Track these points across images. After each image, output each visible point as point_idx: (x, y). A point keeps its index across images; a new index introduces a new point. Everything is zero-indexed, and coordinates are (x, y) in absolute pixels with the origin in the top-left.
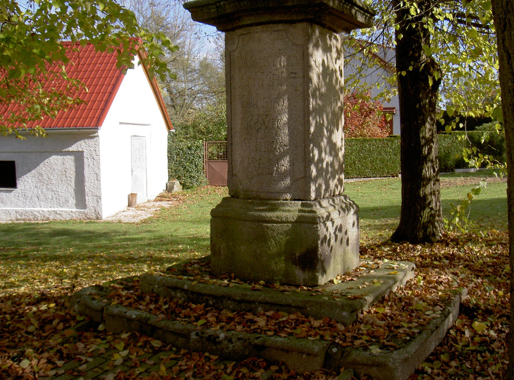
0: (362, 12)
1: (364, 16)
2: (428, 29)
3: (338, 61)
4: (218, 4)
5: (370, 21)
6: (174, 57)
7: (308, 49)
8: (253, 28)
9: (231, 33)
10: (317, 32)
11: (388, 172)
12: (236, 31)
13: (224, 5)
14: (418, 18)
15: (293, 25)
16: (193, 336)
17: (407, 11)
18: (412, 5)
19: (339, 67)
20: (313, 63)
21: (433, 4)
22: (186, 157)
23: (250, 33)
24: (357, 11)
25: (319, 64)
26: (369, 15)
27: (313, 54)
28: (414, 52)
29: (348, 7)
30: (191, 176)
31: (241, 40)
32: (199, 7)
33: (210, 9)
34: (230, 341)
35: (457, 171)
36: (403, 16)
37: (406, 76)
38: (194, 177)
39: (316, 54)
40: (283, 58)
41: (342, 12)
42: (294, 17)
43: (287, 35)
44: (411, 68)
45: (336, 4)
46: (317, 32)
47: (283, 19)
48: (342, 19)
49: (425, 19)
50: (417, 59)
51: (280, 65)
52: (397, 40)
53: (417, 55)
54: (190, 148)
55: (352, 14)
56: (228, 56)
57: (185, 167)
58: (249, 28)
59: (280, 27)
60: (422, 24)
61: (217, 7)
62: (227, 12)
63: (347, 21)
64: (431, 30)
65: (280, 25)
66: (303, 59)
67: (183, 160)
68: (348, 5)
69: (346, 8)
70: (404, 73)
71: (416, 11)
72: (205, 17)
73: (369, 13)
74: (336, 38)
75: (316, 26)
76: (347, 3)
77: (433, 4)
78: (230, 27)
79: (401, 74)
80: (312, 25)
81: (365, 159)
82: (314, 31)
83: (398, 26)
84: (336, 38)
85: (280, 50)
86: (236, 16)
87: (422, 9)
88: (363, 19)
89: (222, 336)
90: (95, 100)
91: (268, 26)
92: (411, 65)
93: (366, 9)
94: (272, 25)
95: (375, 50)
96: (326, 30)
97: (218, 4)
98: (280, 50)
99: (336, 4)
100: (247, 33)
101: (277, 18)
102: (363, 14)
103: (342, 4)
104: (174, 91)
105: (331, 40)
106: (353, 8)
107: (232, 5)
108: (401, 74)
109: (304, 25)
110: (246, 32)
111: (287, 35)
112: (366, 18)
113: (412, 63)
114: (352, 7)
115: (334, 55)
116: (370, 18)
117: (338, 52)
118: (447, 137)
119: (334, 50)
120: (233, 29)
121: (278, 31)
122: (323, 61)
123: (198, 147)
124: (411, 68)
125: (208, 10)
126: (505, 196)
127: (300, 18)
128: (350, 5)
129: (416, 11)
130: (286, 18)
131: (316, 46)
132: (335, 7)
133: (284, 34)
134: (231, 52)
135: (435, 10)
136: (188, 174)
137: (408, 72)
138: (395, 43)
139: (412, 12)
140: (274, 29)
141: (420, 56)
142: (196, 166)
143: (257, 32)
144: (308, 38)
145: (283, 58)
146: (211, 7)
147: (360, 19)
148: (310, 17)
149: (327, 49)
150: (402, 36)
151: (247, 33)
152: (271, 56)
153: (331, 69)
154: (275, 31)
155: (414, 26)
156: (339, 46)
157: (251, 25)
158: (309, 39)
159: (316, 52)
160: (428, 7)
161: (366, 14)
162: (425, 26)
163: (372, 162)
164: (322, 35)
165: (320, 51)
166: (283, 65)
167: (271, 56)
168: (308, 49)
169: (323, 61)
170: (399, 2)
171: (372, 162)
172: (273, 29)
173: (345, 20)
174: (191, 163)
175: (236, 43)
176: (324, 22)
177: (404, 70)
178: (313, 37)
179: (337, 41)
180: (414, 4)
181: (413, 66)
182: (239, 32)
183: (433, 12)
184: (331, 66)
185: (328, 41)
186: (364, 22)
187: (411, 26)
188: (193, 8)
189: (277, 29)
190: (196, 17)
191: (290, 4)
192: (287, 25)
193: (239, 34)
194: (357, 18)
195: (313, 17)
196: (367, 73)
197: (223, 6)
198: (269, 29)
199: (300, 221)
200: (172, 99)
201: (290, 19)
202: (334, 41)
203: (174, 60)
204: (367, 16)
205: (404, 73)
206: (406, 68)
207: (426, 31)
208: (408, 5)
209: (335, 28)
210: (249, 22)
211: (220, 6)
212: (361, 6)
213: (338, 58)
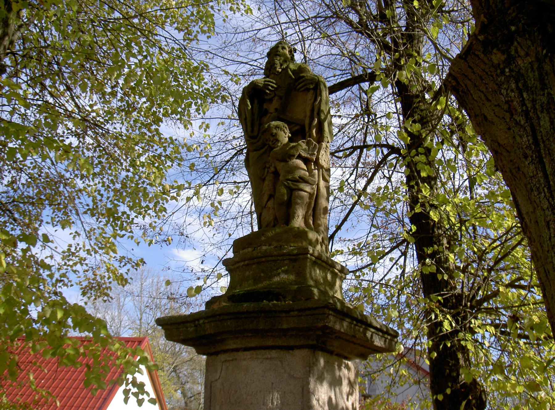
0: (381, 334)
1: (383, 339)
2: (466, 346)
3: (350, 397)
4: (197, 322)
5: (391, 344)
6: (191, 356)
7: (309, 384)
8: (240, 354)
9: (213, 357)
10: (322, 362)
12: (219, 356)
13: (204, 323)
14: (455, 333)
15: (291, 351)
17: (441, 324)
18: (445, 318)
19: (353, 404)
20: (315, 402)
21: (471, 316)
23: (236, 359)
24: (373, 333)
25: (324, 403)
26: (389, 337)
27: (314, 391)
28: (451, 371)
29: (361, 330)
31: (224, 367)
32: (174, 324)
33: (187, 328)
36: (437, 329)
37: (443, 400)
39: (320, 389)
40: (276, 395)
41: (354, 336)
42: (292, 342)
43: (282, 363)
44: (448, 391)
45: (345, 327)
46: (322, 362)
47: (277, 344)
48: (355, 344)
49: (461, 335)
50: (456, 379)
51: (272, 403)
52: (430, 359)
53: (455, 374)
55: (367, 338)
56: (209, 387)
58: (236, 353)
59: (274, 353)
60: (459, 341)
61: (196, 326)
62: (207, 333)
63: (362, 346)
64: (470, 346)
65: (274, 351)
66: (303, 396)
68: (361, 327)
69: (359, 331)
70: (440, 397)
71: (451, 325)
72: (182, 337)
73: (389, 334)
74: (349, 369)
75: (320, 353)
76: (359, 324)
77: (471, 316)
78: (213, 350)
79: (437, 398)
80: (314, 352)
82: (317, 360)
83: (431, 343)
84: (349, 369)
85: (273, 383)
86: (218, 338)
87: (457, 322)
88: (382, 343)
90: (86, 406)
91: (259, 352)
92: (449, 387)
93: (385, 330)
94: (263, 352)
95: (403, 371)
96: (335, 357)
97: (197, 322)
98: (273, 383)
99: (345, 327)
100: (232, 360)
101: (270, 342)
102: (382, 337)
103: (353, 326)
104: (189, 395)
105: (340, 369)
106: (368, 330)
107: (213, 324)
108: (437, 398)
109: (304, 353)
110: (231, 359)
111: (282, 363)
112: (385, 341)
113: (450, 384)
114: (366, 330)
115: (345, 388)
116: (391, 340)
117: (351, 385)
119: (345, 382)
120: (217, 353)
121: (271, 359)
122: (330, 399)
124: (448, 391)
125: (185, 329)
127: (298, 343)
128: (363, 326)
129: (451, 325)
130: (280, 342)
131: (320, 379)
132: (342, 330)
133: (279, 363)
134: (212, 382)
135: (473, 322)
137: (445, 395)
138: (428, 362)
139: (446, 326)
140: (266, 356)
141: (458, 375)
143: (244, 360)
144: (310, 367)
145: (276, 395)
146: (188, 324)
147: (378, 342)
148: (311, 342)
149: (336, 383)
150: (436, 354)
151: (232, 360)
152: (260, 391)
153: (340, 407)
154: (267, 359)
155: (449, 345)
156: (352, 376)
157: (237, 350)
158: (310, 371)
159: (319, 386)
160: (465, 318)
161: (386, 336)
162: (463, 343)
164: (329, 367)
165: (325, 386)
166: (275, 403)
167: (260, 391)
168: (308, 383)
169: (330, 399)
170: (430, 314)
172: (264, 357)
173: (359, 344)
175: (219, 371)
176: (331, 348)
177: (440, 393)
178: (315, 368)
179: (349, 370)
180: (448, 316)
181: (451, 388)
182: (222, 357)
183: (472, 326)
184: (342, 404)
185: (337, 373)
186: (384, 346)
187: (445, 345)
188: (167, 324)
189: (269, 356)
190: (169, 337)
191: (285, 326)
192: (282, 352)
193: (223, 360)
194: (374, 342)
195: (315, 342)
196: (398, 391)
197: (203, 326)
198: (259, 357)
200: (186, 403)
201: (286, 344)
202: (345, 371)
203: (191, 359)
204: (386, 338)
205: (440, 397)
206: (442, 392)
207: (464, 350)
208: (440, 318)
209: (346, 354)
210: (235, 346)
211: (199, 324)
212: (379, 327)
213: (350, 394)
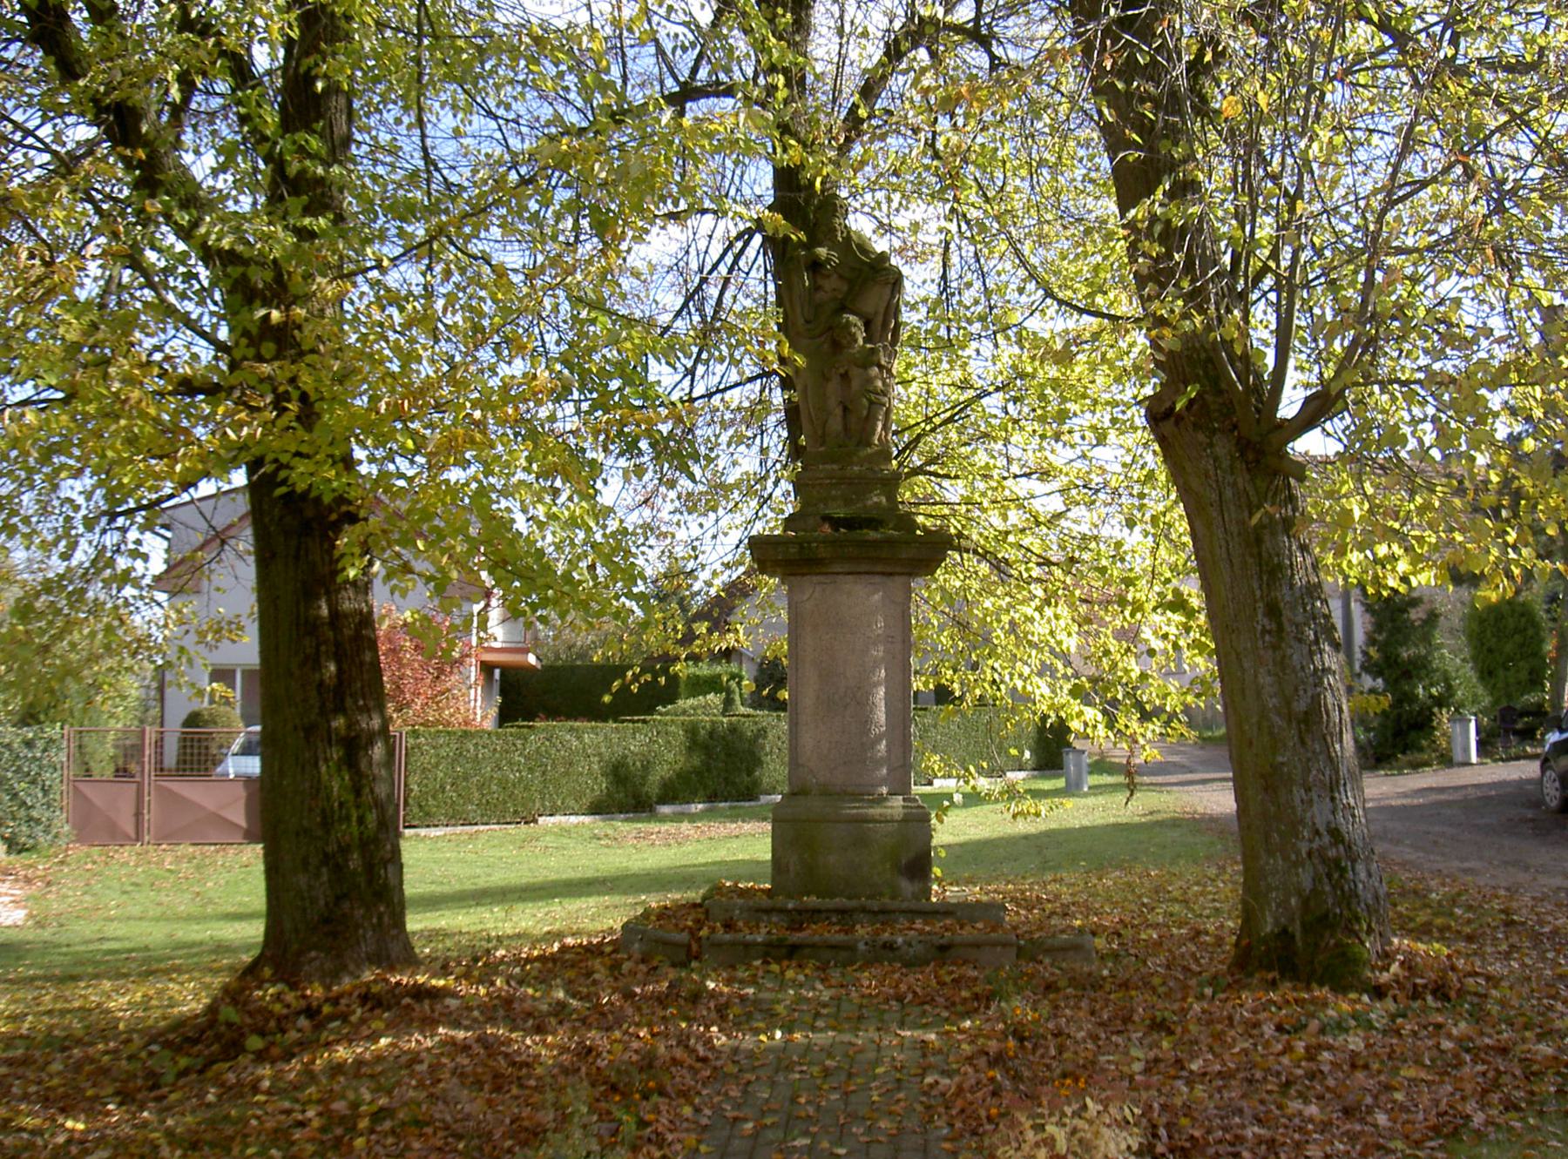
11: (516, 812)
16: (861, 946)
22: (19, 768)
30: (30, 819)
34: (910, 945)
35: (666, 809)
38: (38, 821)
54: (29, 744)
57: (16, 795)
59: (877, 579)
67: (10, 775)
81: (466, 779)
89: (900, 940)
118: (639, 730)
123: (51, 741)
126: (769, 856)
136: (22, 813)
142: (45, 792)
163: (481, 787)
171: (481, 787)
174: (33, 782)
199: (906, 819)
